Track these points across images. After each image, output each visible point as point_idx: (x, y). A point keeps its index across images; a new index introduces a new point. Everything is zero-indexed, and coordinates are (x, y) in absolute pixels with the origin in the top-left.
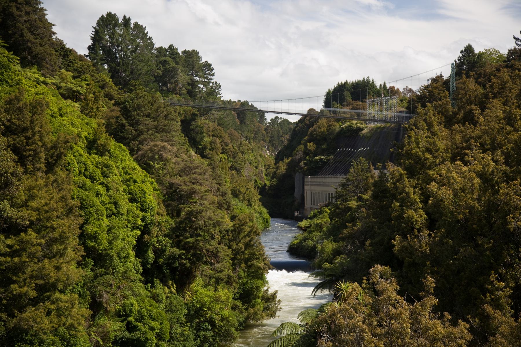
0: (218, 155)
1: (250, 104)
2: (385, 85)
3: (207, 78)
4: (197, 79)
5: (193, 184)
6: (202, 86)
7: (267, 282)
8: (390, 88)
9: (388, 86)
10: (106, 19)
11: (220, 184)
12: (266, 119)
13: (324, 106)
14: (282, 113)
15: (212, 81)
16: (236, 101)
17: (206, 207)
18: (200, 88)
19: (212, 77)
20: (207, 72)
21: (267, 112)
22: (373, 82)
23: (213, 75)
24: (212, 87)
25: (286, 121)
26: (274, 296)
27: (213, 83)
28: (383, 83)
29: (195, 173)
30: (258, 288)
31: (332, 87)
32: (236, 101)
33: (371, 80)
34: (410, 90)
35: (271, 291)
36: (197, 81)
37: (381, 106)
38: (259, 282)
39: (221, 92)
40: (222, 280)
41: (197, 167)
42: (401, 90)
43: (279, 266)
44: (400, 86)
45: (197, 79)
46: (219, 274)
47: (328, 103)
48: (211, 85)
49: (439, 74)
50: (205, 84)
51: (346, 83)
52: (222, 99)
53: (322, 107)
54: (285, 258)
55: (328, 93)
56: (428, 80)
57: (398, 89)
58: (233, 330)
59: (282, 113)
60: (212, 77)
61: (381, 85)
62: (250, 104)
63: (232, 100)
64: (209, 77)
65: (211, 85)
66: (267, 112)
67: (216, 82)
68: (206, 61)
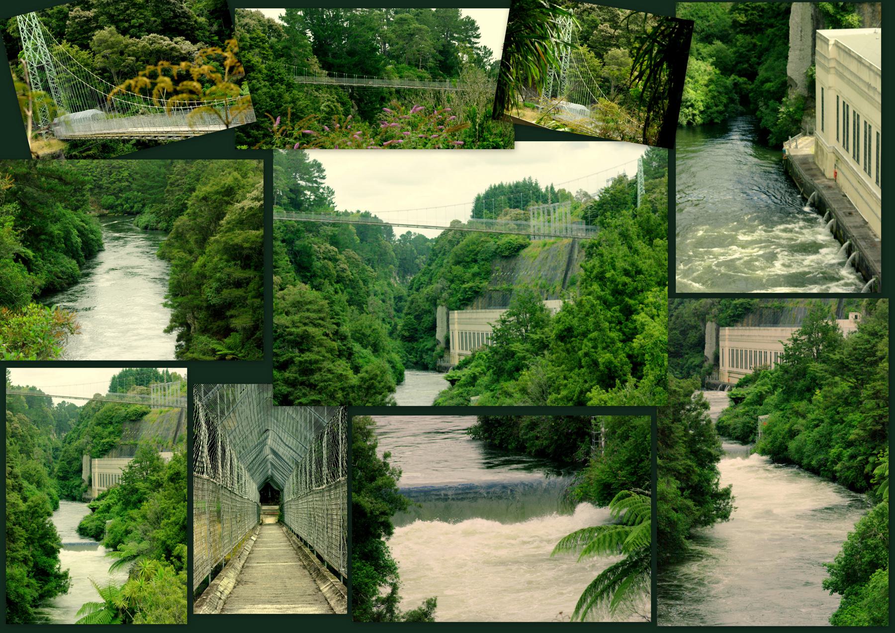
0: (332, 285)
1: (373, 215)
2: (552, 188)
3: (316, 182)
4: (302, 183)
5: (305, 324)
6: (308, 193)
7: (59, 561)
8: (560, 191)
9: (556, 190)
10: (287, 31)
11: (338, 324)
12: (394, 236)
13: (473, 217)
14: (418, 226)
15: (323, 186)
16: (355, 212)
17: (324, 356)
18: (306, 195)
19: (322, 181)
20: (317, 174)
21: (398, 225)
22: (536, 184)
23: (324, 178)
24: (322, 193)
25: (73, 406)
26: (66, 575)
27: (324, 188)
28: (549, 186)
29: (308, 310)
30: (52, 567)
31: (482, 190)
32: (355, 212)
33: (534, 181)
34: (586, 194)
35: (62, 571)
36: (302, 186)
37: (549, 215)
38: (51, 561)
39: (334, 201)
40: (18, 559)
41: (310, 303)
42: (574, 194)
43: (71, 546)
44: (573, 190)
45: (302, 183)
46: (15, 554)
47: (477, 213)
48: (321, 190)
49: (621, 173)
50: (314, 190)
51: (501, 186)
52: (336, 209)
53: (469, 218)
54: (76, 539)
55: (478, 199)
56: (608, 181)
57: (569, 193)
58: (28, 606)
59: (418, 226)
60: (322, 181)
61: (547, 188)
62: (373, 215)
63: (349, 211)
64: (319, 180)
65: (321, 190)
66: (398, 225)
67: (328, 188)
68: (314, 160)
